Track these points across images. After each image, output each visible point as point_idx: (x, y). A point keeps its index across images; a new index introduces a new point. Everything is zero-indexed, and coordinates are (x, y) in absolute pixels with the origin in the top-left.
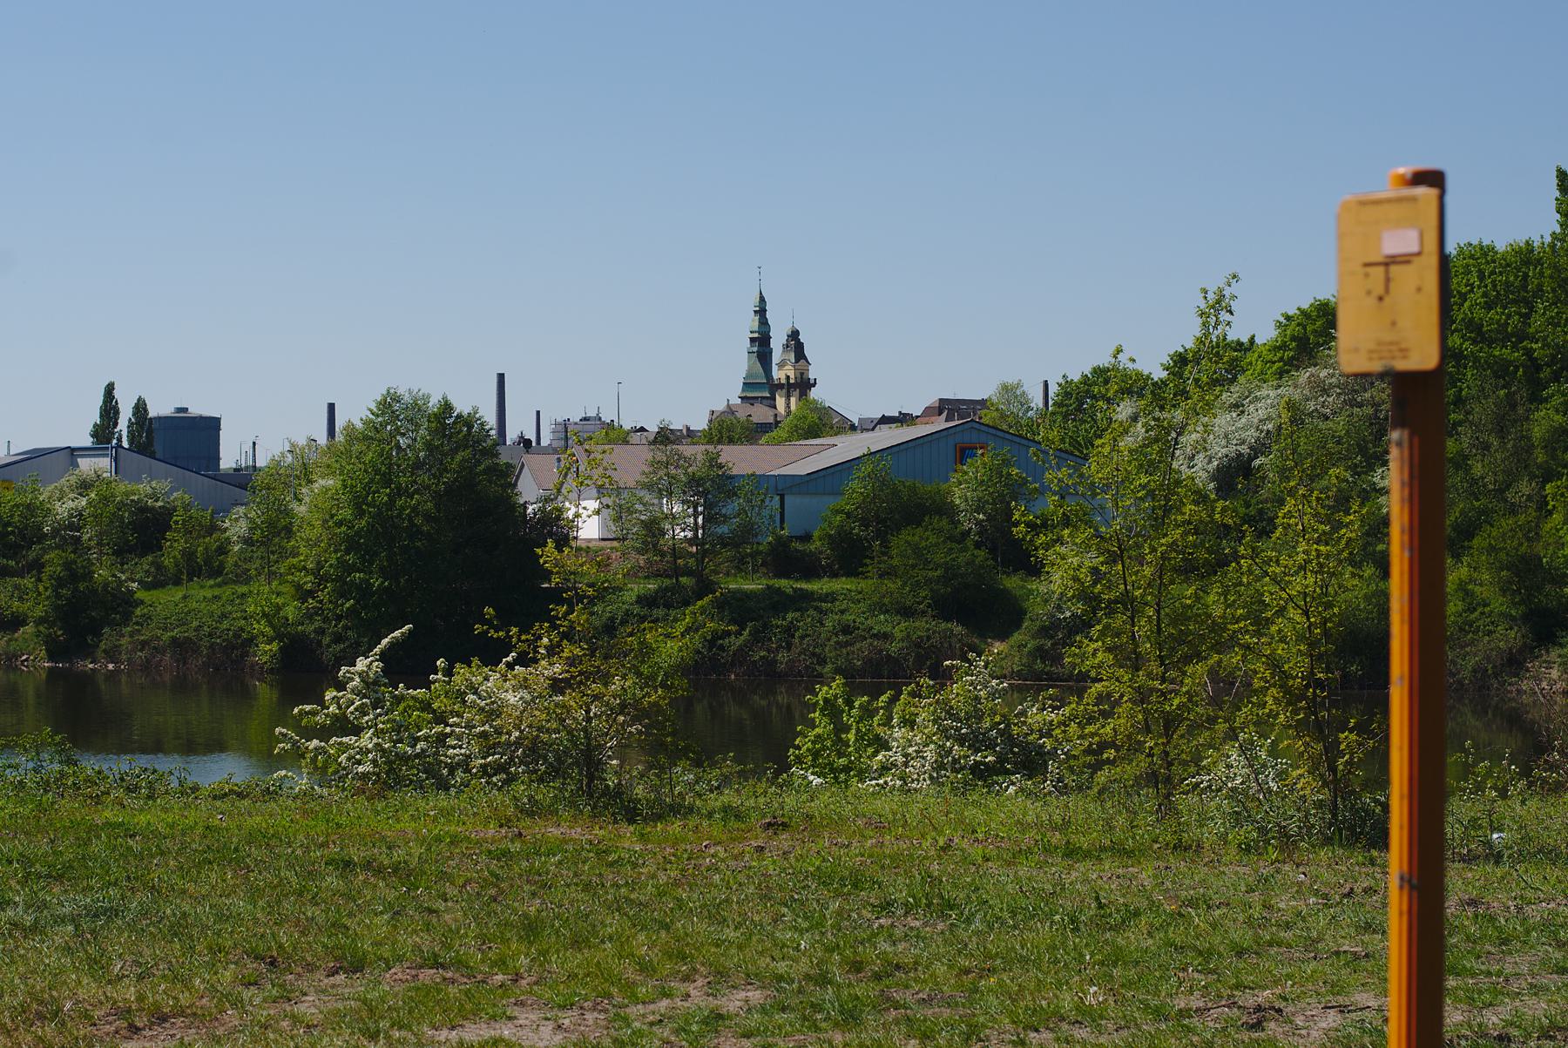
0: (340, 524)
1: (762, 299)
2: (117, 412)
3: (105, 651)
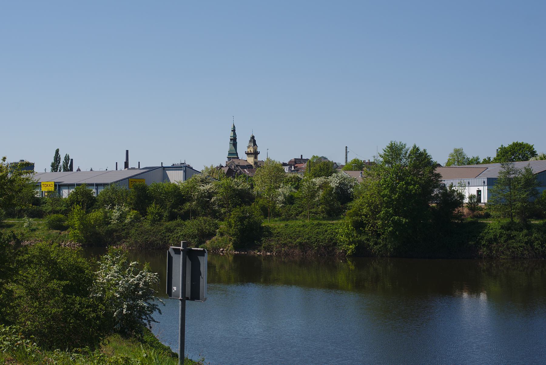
0: (383, 196)
1: (234, 127)
2: (60, 159)
3: (264, 247)
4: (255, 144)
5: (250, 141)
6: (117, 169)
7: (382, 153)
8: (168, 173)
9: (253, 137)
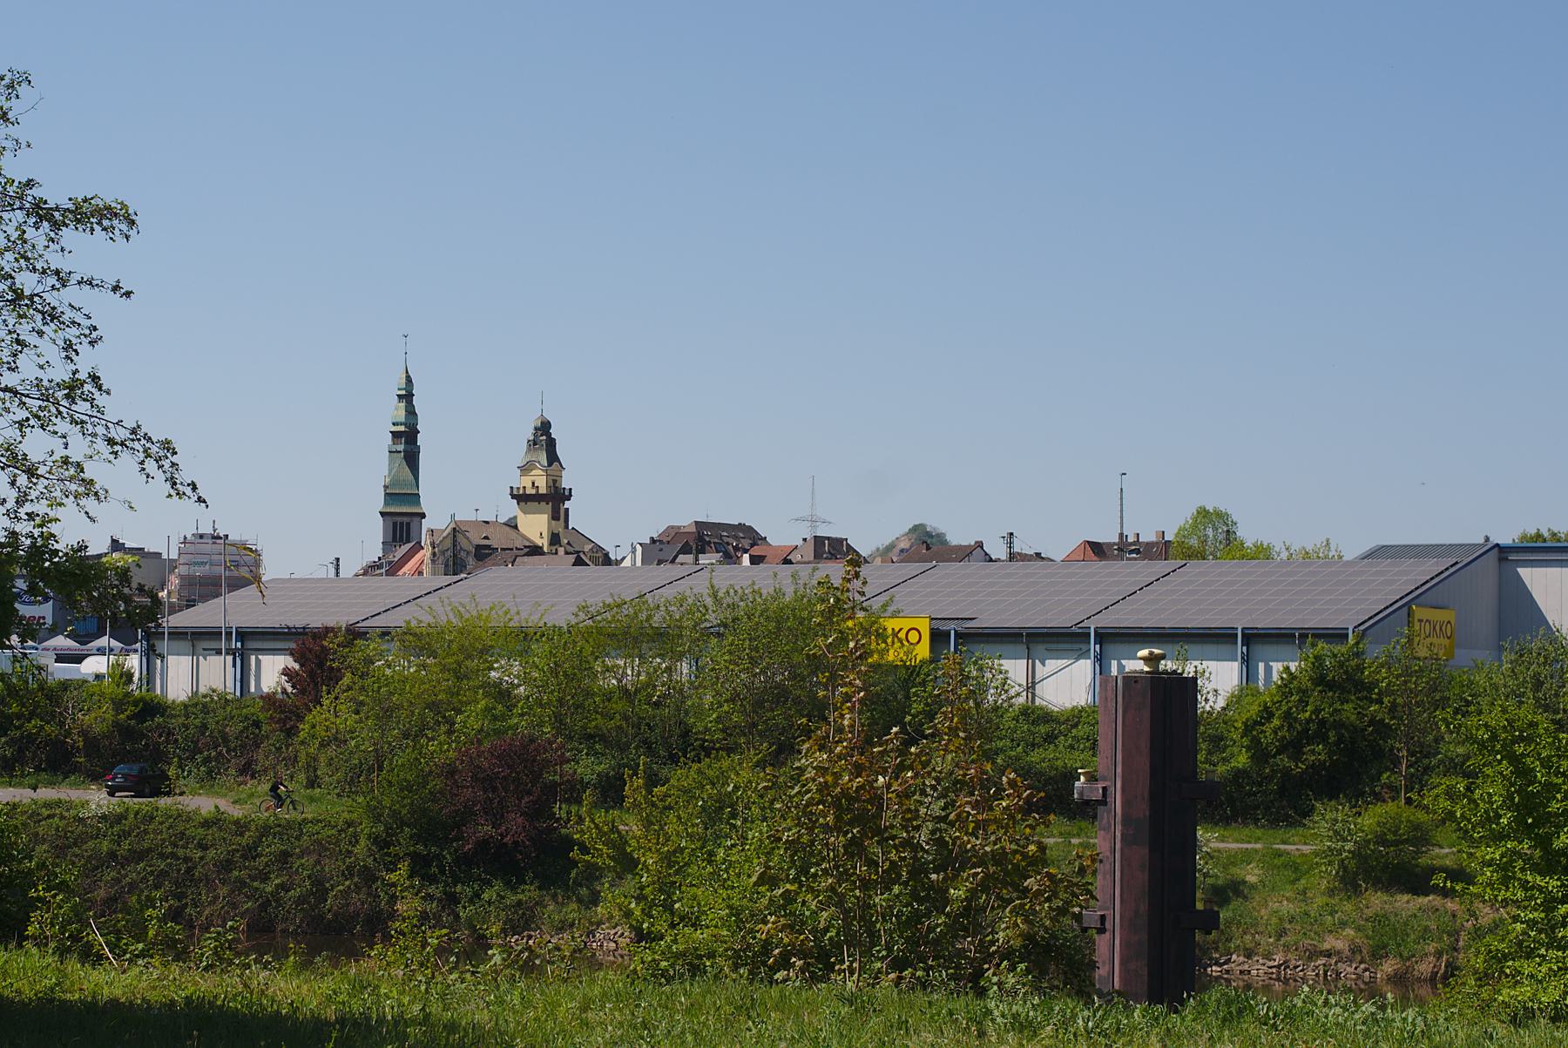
1: (409, 380)
4: (553, 458)
5: (534, 443)
6: (337, 574)
7: (1295, 547)
8: (1532, 577)
9: (544, 428)
